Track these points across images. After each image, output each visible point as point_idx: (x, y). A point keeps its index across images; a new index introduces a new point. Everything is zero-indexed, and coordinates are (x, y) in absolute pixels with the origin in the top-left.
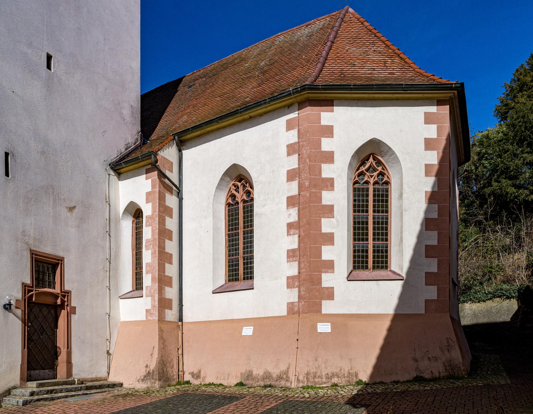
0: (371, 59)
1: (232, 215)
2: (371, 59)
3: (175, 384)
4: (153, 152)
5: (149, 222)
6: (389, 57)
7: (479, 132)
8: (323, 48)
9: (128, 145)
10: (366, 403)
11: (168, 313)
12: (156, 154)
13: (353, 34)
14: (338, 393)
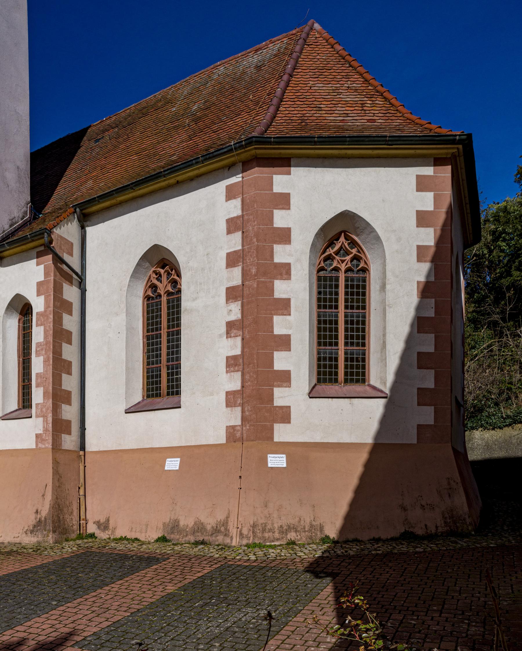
0: (343, 99)
1: (153, 318)
2: (343, 99)
3: (75, 537)
4: (46, 229)
5: (41, 321)
6: (369, 96)
7: (494, 203)
8: (277, 84)
9: (14, 221)
10: (333, 570)
11: (65, 438)
12: (51, 232)
13: (319, 62)
14: (296, 554)
